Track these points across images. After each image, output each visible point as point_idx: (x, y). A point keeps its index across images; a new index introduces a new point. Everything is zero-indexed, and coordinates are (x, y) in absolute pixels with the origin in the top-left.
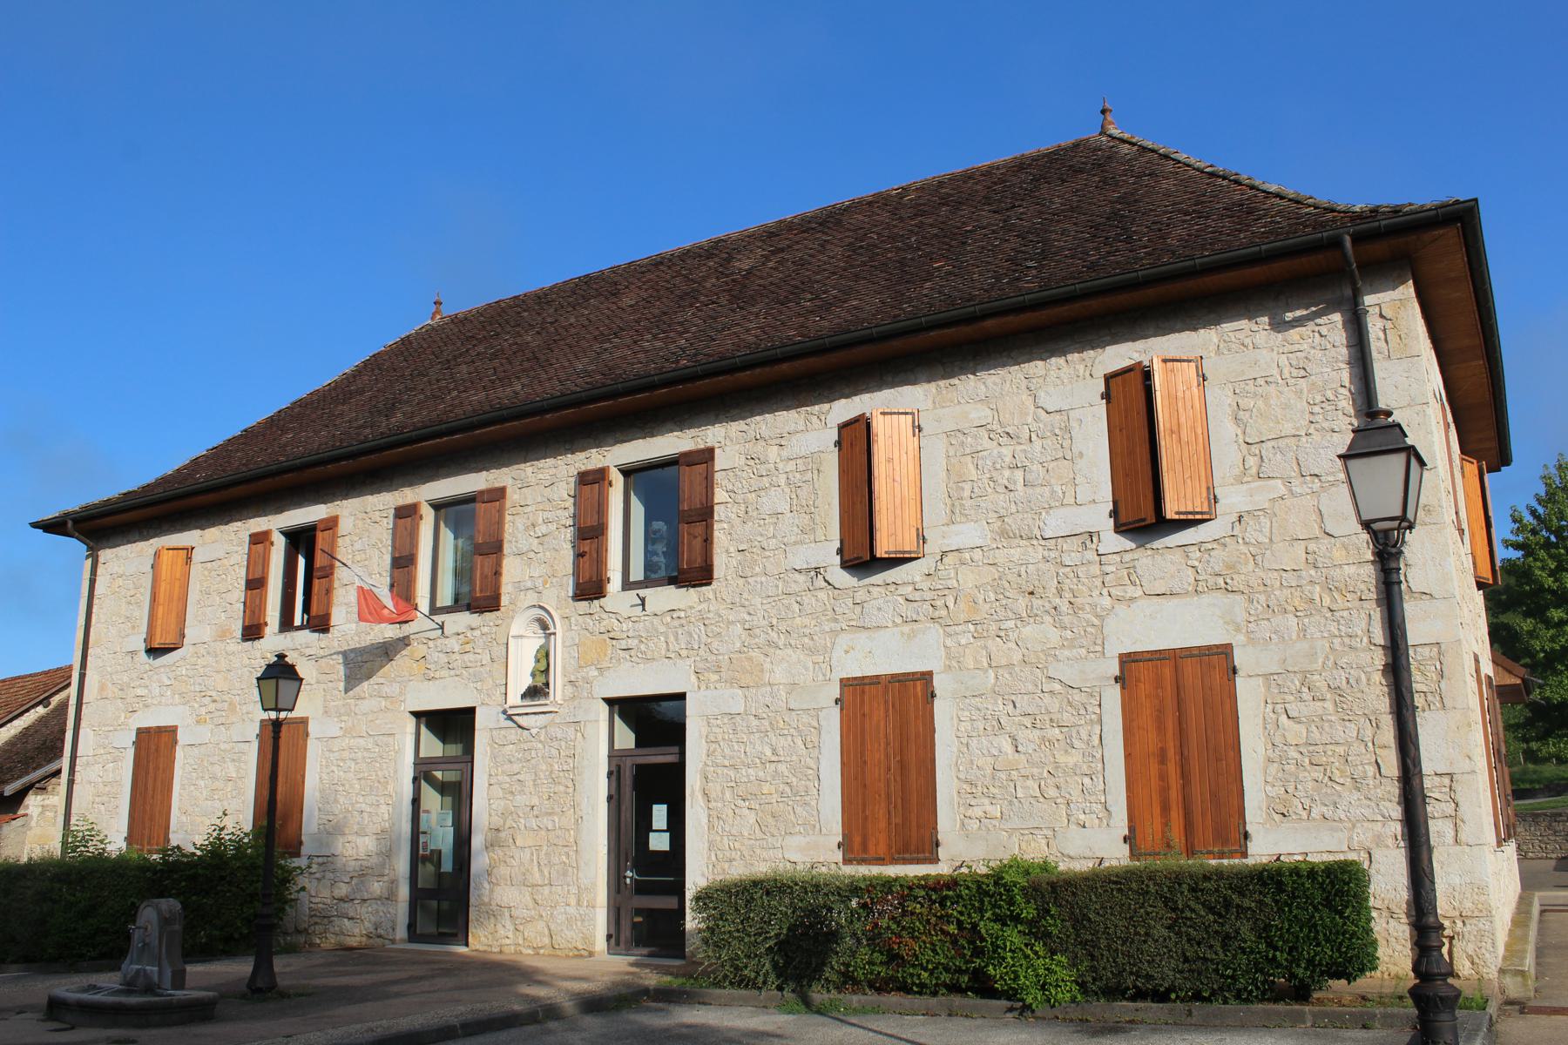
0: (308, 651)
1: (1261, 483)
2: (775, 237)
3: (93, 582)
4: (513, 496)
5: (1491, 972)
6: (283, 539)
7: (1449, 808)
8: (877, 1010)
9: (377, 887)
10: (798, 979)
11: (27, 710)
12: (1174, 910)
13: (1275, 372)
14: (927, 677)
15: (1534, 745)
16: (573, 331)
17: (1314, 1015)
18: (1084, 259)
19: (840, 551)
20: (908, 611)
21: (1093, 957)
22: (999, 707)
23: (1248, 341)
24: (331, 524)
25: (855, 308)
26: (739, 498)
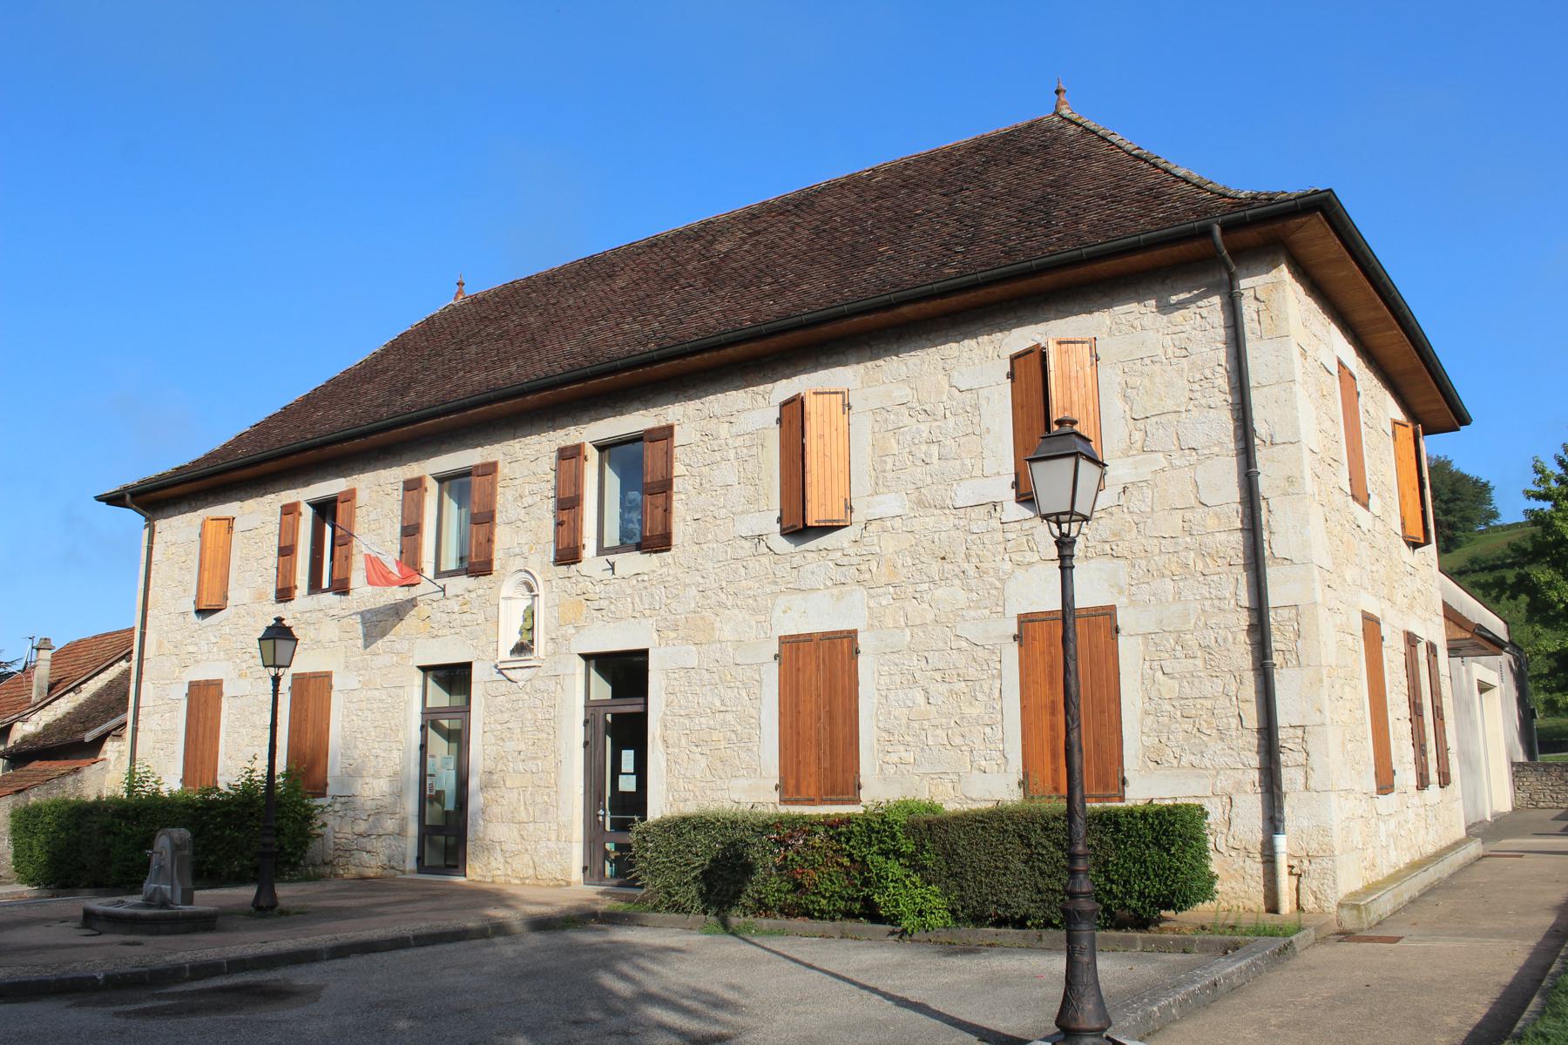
0: (332, 612)
1: (1146, 456)
2: (754, 220)
3: (150, 549)
4: (504, 470)
5: (1331, 907)
6: (310, 510)
7: (1301, 758)
8: (782, 933)
9: (390, 824)
10: (720, 905)
11: (112, 665)
12: (1029, 846)
13: (1160, 352)
14: (852, 635)
15: (1557, 696)
16: (570, 312)
17: (1144, 941)
18: (1013, 240)
19: (780, 520)
20: (837, 574)
21: (962, 888)
22: (915, 663)
23: (1136, 323)
24: (350, 496)
25: (805, 292)
26: (695, 471)
